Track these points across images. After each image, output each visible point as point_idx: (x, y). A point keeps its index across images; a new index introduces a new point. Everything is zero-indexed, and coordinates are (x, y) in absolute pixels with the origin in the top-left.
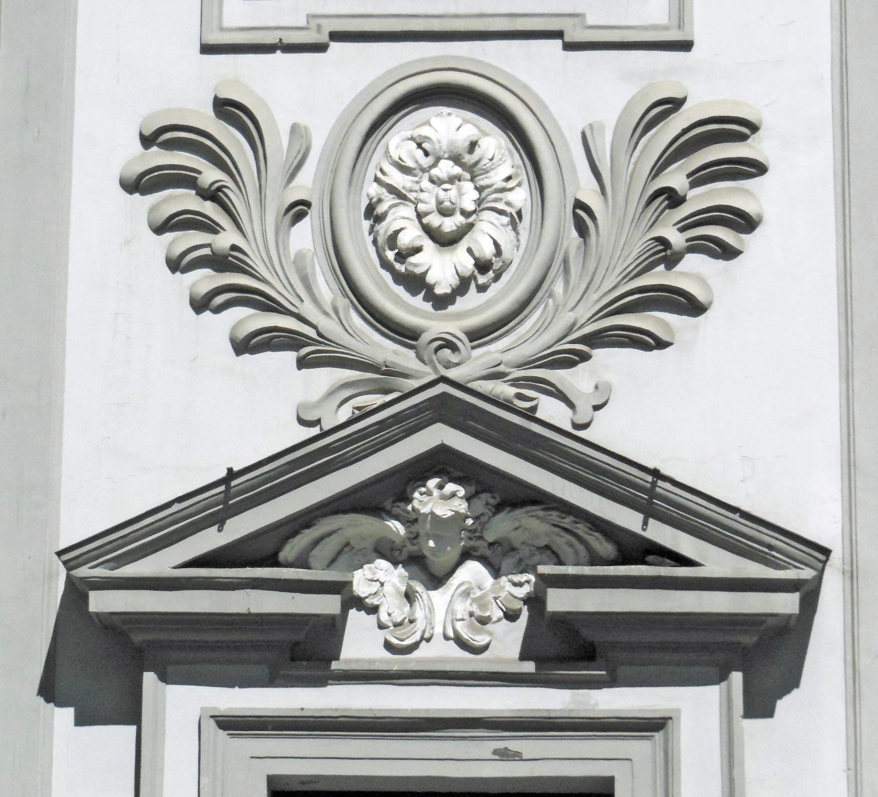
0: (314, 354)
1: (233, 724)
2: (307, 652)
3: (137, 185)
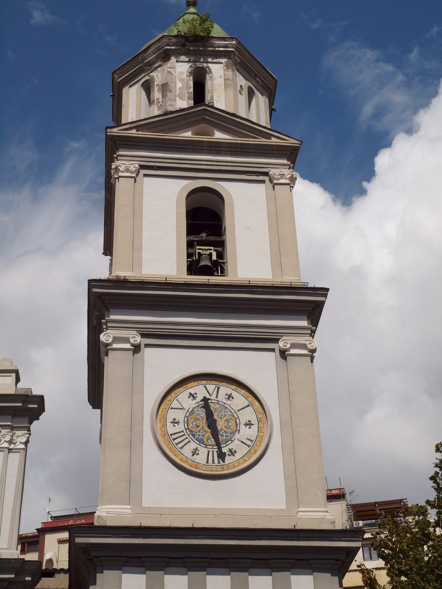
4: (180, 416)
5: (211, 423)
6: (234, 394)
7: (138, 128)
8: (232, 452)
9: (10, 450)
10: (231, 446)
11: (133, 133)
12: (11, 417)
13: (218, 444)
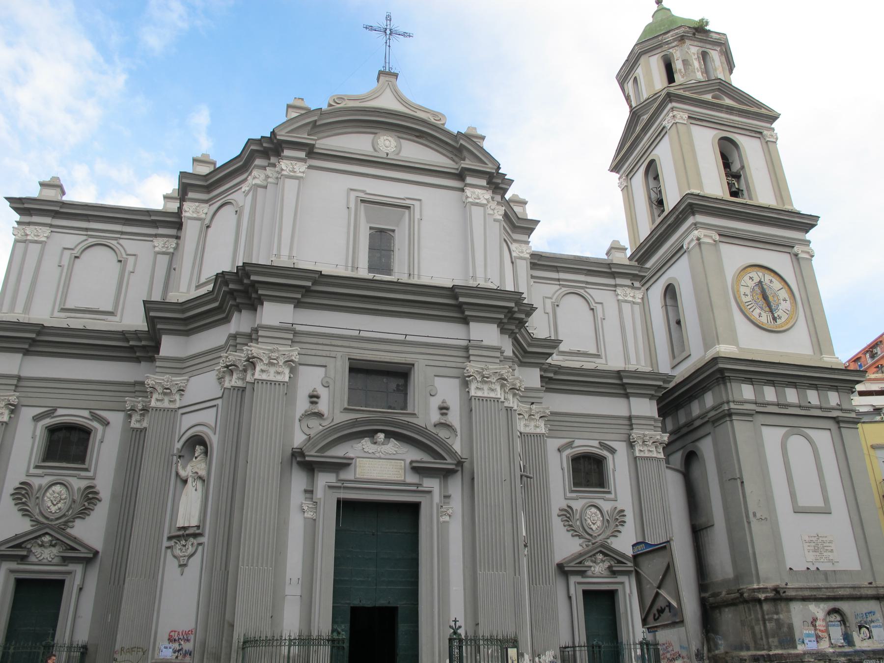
0: (580, 537)
1: (579, 583)
2: (23, 559)
3: (12, 495)
4: (748, 292)
5: (765, 297)
6: (774, 280)
7: (685, 89)
8: (780, 318)
9: (634, 303)
10: (778, 313)
11: (681, 92)
12: (21, 355)
13: (771, 311)
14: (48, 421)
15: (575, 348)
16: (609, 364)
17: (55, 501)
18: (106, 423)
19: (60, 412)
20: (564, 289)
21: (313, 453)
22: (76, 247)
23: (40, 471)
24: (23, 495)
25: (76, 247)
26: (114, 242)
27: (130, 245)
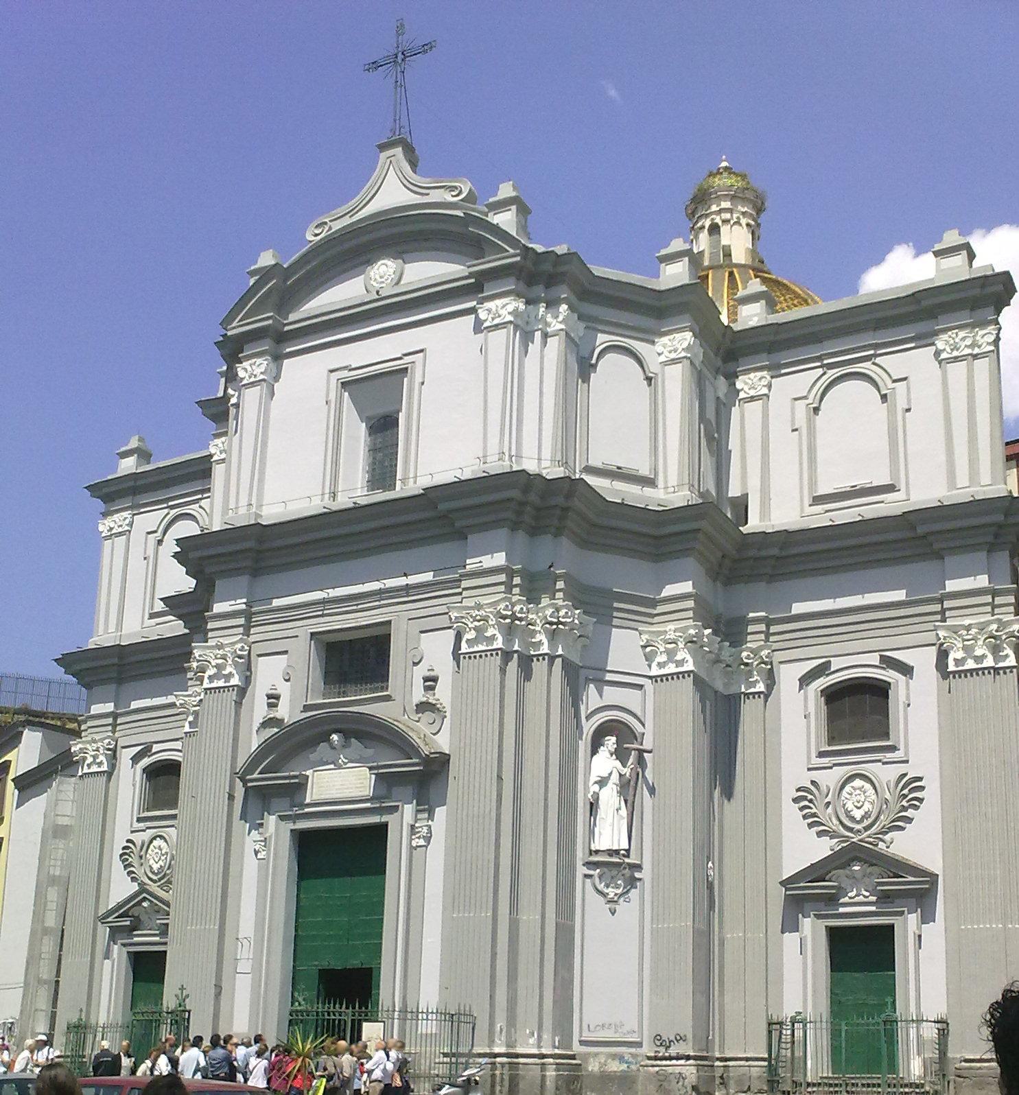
12: (113, 686)
14: (146, 762)
15: (844, 484)
16: (913, 498)
17: (860, 801)
18: (906, 670)
19: (156, 748)
20: (830, 372)
21: (255, 776)
22: (158, 528)
23: (825, 761)
24: (811, 801)
25: (158, 528)
26: (868, 364)
27: (894, 363)
